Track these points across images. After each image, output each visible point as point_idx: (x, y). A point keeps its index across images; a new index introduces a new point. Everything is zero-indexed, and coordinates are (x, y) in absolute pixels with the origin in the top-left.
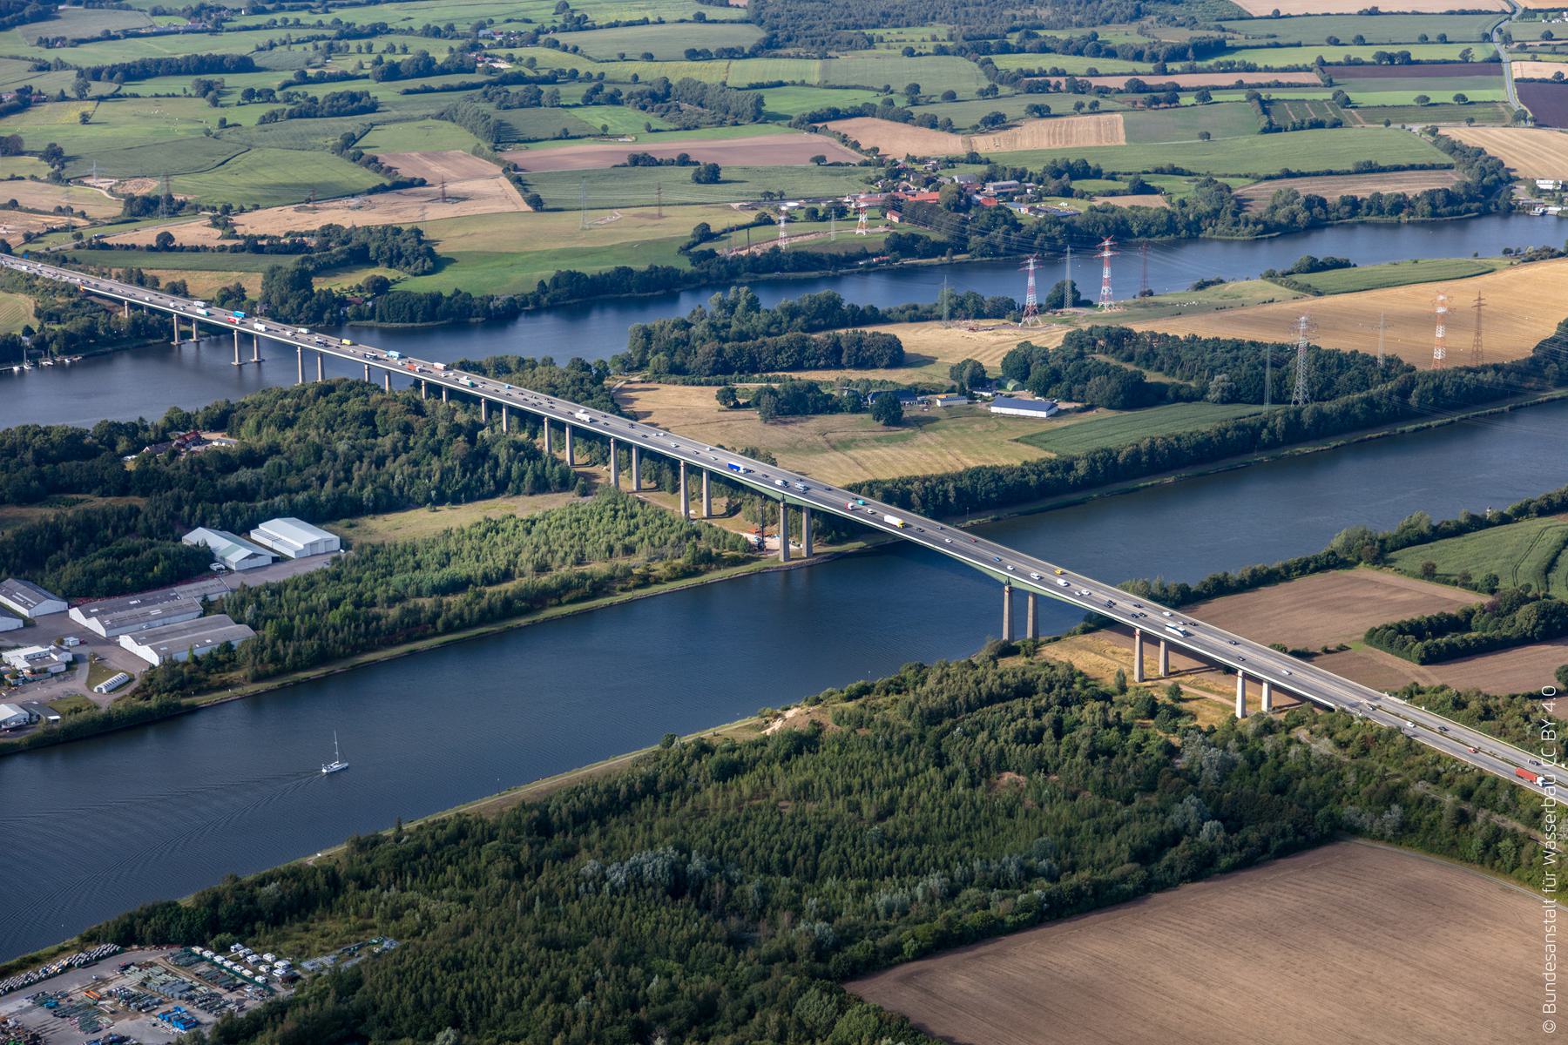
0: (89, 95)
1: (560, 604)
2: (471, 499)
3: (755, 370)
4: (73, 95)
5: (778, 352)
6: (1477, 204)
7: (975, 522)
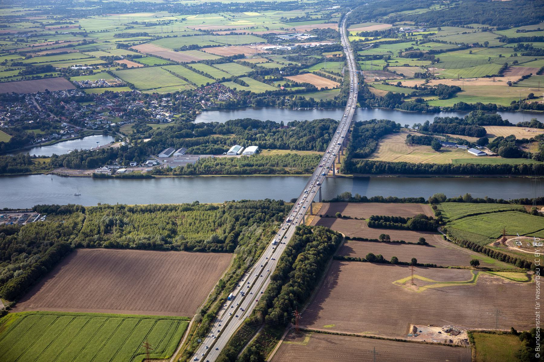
0: (489, 46)
1: (259, 174)
2: (303, 150)
3: (443, 133)
4: (484, 46)
5: (449, 128)
6: (340, 78)
7: (391, 176)
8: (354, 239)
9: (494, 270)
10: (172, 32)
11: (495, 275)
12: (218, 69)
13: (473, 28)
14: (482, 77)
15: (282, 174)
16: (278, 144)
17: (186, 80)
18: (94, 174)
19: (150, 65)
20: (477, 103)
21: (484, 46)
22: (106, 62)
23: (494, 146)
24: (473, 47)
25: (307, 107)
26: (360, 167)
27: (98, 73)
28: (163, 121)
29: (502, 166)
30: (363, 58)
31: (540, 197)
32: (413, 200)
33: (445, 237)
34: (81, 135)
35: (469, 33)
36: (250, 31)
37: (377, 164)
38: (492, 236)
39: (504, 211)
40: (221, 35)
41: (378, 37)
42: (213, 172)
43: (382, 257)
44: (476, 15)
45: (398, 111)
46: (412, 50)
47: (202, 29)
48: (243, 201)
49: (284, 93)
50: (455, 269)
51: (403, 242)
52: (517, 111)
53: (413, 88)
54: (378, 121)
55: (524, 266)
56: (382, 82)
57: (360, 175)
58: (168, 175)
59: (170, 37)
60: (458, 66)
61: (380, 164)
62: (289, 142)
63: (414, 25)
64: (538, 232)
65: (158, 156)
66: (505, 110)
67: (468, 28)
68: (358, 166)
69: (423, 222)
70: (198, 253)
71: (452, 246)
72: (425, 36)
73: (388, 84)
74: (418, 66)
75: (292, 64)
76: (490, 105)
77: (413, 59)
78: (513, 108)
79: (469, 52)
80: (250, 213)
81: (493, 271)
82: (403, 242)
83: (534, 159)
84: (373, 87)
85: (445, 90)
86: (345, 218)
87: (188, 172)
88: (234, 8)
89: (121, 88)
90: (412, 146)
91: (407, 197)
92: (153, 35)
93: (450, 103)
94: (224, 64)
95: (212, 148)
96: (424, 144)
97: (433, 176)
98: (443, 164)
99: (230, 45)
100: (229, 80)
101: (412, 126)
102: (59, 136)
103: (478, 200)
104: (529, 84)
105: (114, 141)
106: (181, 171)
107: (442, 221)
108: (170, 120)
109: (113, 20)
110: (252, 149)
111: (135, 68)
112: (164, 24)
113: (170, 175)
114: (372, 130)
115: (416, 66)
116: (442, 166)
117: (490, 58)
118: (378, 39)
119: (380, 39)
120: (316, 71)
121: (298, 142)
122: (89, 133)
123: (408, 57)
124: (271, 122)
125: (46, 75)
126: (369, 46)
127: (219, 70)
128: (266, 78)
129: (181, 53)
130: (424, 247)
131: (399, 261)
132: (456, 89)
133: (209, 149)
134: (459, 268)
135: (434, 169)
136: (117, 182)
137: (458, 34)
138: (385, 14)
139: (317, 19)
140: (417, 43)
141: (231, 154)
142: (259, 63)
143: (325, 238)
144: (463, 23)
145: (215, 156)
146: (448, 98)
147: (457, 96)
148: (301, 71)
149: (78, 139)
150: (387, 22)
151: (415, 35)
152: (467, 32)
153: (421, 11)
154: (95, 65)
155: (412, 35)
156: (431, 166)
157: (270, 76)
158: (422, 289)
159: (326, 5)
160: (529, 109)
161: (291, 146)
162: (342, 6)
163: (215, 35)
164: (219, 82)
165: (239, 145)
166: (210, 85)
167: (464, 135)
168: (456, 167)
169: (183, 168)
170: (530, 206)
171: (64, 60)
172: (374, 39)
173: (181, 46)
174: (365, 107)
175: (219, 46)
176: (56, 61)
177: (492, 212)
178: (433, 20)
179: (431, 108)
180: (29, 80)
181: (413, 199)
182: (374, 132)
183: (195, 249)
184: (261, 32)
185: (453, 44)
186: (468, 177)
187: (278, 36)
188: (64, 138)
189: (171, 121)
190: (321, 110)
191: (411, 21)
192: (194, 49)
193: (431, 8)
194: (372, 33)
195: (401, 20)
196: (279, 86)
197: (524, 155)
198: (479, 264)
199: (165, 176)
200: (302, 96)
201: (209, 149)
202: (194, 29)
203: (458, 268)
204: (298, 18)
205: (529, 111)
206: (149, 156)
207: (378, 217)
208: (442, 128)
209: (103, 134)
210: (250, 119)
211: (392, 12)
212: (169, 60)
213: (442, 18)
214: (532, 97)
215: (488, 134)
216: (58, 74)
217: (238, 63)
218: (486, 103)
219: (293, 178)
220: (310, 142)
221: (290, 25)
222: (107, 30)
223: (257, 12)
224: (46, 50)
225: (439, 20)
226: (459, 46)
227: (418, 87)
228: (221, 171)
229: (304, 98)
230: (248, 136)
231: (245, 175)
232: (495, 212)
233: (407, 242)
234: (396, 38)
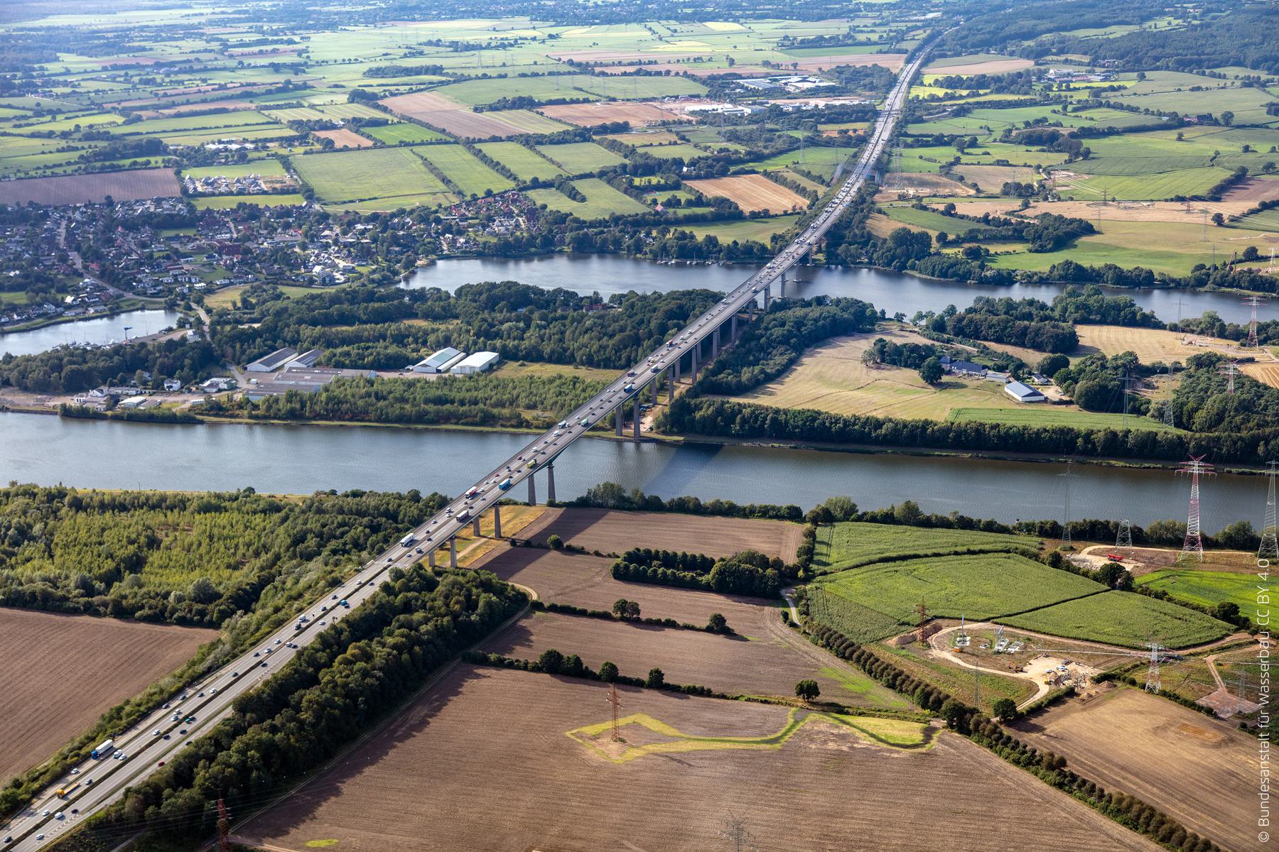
0: (1233, 123)
1: (457, 424)
2: (606, 367)
3: (978, 338)
4: (1222, 122)
5: (990, 328)
7: (776, 445)
8: (554, 608)
9: (851, 710)
10: (504, 65)
11: (848, 724)
12: (544, 156)
13: (1224, 77)
14: (1166, 200)
15: (512, 426)
16: (547, 349)
17: (446, 181)
18: (64, 406)
19: (388, 143)
20: (1106, 265)
21: (1222, 122)
22: (296, 134)
23: (1069, 379)
24: (1196, 124)
25: (691, 258)
26: (703, 417)
27: (259, 159)
28: (324, 280)
29: (1054, 431)
30: (909, 140)
31: (1088, 520)
32: (771, 513)
33: (786, 616)
34: (111, 309)
35: (1207, 89)
36: (681, 68)
37: (746, 411)
38: (906, 620)
39: (982, 552)
40: (612, 75)
41: (981, 92)
42: (346, 413)
43: (578, 660)
44: (1246, 45)
45: (912, 277)
46: (1043, 126)
47: (576, 59)
48: (356, 494)
49: (655, 221)
50: (755, 704)
51: (671, 624)
52: (1202, 289)
53: (978, 220)
54: (831, 301)
55: (930, 704)
56: (914, 202)
57: (701, 439)
58: (237, 416)
59: (490, 77)
60: (1127, 170)
61: (753, 412)
62: (576, 345)
63: (1089, 64)
64: (1028, 614)
65: (246, 369)
66: (1172, 285)
67: (1214, 76)
68: (698, 415)
69: (745, 570)
70: (142, 626)
71: (795, 638)
72: (1097, 92)
73: (925, 208)
74: (1030, 166)
75: (728, 150)
76: (1137, 272)
77: (1029, 148)
78: (1192, 282)
79: (1176, 136)
80: (341, 525)
81: (847, 713)
82: (671, 624)
83: (1153, 416)
84: (885, 214)
85: (1051, 230)
86: (572, 550)
87: (283, 412)
88: (689, 11)
89: (286, 196)
90: (878, 368)
91: (759, 502)
92: (450, 71)
93: (1043, 263)
94: (568, 145)
95: (378, 354)
96: (906, 366)
97: (881, 449)
98: (909, 418)
99: (614, 100)
100: (547, 185)
101: (912, 317)
102: (59, 310)
103: (934, 518)
104: (1270, 224)
105: (175, 327)
106: (269, 407)
107: (807, 570)
108: (342, 279)
109: (391, 35)
110: (480, 359)
111: (351, 150)
112: (503, 46)
113: (242, 417)
114: (795, 323)
115: (1025, 165)
116: (905, 426)
117: (1217, 153)
118: (980, 95)
119: (986, 94)
120: (769, 169)
121: (595, 348)
122: (133, 304)
123: (1020, 143)
124: (567, 292)
125: (135, 163)
126: (945, 111)
127: (544, 160)
128: (637, 181)
129: (487, 115)
130: (720, 639)
131: (621, 674)
132: (1079, 226)
133: (372, 354)
134: (766, 702)
135: (883, 432)
136: (119, 428)
137: (1180, 90)
138: (1030, 35)
139: (869, 43)
140: (1065, 108)
141: (424, 369)
142: (651, 145)
143: (458, 602)
144: (1206, 64)
145: (379, 373)
146: (1051, 250)
147: (1075, 246)
148: (733, 169)
149: (101, 317)
150: (1026, 54)
151: (1075, 89)
152: (1204, 87)
153: (1118, 32)
154: (260, 140)
155: (1068, 89)
156: (879, 424)
157: (647, 178)
158: (633, 754)
159: (914, 9)
160: (1233, 287)
161: (578, 356)
162: (945, 13)
163: (598, 75)
164: (521, 190)
165: (456, 348)
166: (494, 196)
167: (1023, 345)
168: (939, 430)
169: (277, 400)
170: (1057, 541)
171: (206, 128)
172: (968, 96)
173: (493, 98)
174: (837, 265)
175: (586, 101)
176: (185, 130)
177: (949, 554)
178: (1137, 53)
179: (988, 273)
180: (92, 173)
181: (773, 508)
182: (799, 329)
183: (138, 614)
184: (704, 71)
185: (1153, 113)
186: (967, 455)
187: (741, 81)
188: (69, 314)
189: (345, 282)
190: (729, 268)
191: (1085, 53)
192: (521, 107)
193: (1146, 25)
194: (972, 79)
195: (1061, 52)
196: (655, 202)
197: (1134, 407)
198: (818, 694)
199: (228, 420)
200: (687, 230)
201: (372, 354)
202: (560, 60)
203: (762, 702)
204: (821, 38)
205: (1229, 293)
206: (224, 367)
207: (648, 552)
208: (976, 326)
209: (164, 309)
210: (515, 284)
211: (1049, 31)
212: (444, 131)
213: (1160, 49)
214: (1252, 255)
215: (1084, 347)
216: (164, 161)
217: (600, 143)
218: (1127, 266)
219: (506, 439)
220: (625, 347)
221: (790, 54)
222: (356, 60)
223: (738, 22)
224: (188, 103)
225: (1149, 54)
226: (1165, 119)
227: (990, 218)
228: (367, 413)
229: (692, 237)
230: (481, 327)
231: (420, 426)
232: (956, 553)
233: (680, 622)
234: (1026, 94)
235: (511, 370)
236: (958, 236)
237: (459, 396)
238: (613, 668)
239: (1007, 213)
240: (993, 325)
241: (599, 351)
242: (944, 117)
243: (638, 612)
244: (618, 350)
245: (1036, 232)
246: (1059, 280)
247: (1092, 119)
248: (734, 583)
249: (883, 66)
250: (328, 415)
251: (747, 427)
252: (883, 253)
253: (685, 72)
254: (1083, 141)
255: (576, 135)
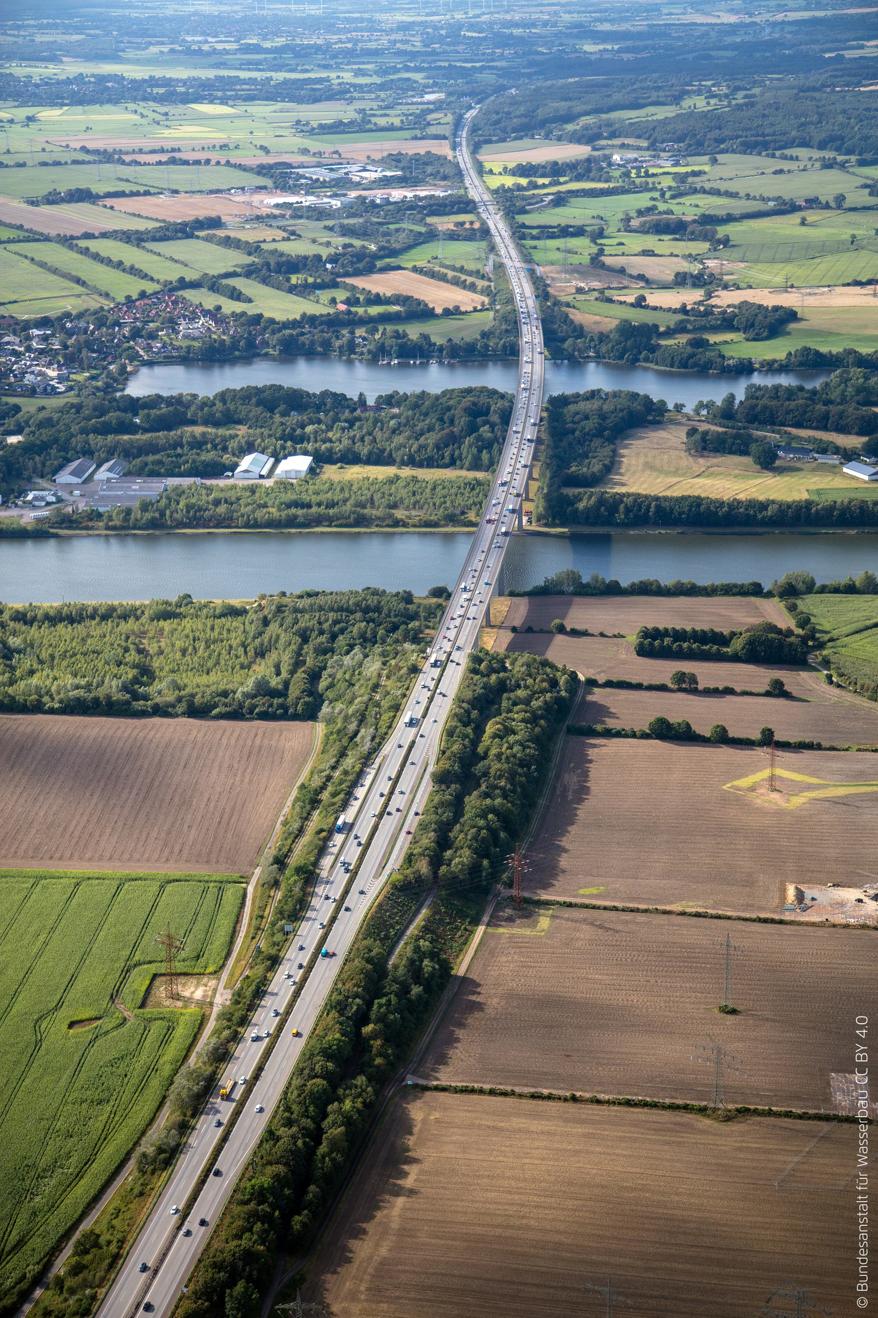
0: (845, 206)
1: (330, 526)
4: (833, 204)
5: (788, 413)
7: (663, 532)
14: (844, 285)
15: (388, 526)
20: (845, 350)
21: (833, 204)
25: (414, 357)
26: (586, 508)
28: (45, 389)
32: (734, 590)
35: (789, 171)
37: (628, 501)
40: (145, 164)
41: (562, 179)
42: (210, 520)
44: (803, 125)
45: (646, 369)
46: (653, 214)
49: (349, 320)
53: (675, 311)
57: (587, 530)
58: (92, 528)
60: (778, 256)
61: (635, 501)
68: (581, 505)
72: (682, 178)
73: (610, 301)
74: (677, 256)
82: (729, 691)
88: (161, 91)
94: (171, 242)
95: (194, 461)
96: (731, 452)
98: (790, 500)
99: (176, 192)
110: (299, 464)
115: (672, 255)
117: (854, 237)
118: (560, 184)
119: (565, 183)
121: (415, 447)
123: (647, 233)
126: (542, 201)
130: (781, 702)
131: (731, 735)
135: (769, 513)
137: (763, 173)
138: (570, 118)
139: (391, 128)
144: (772, 145)
147: (789, 333)
152: (786, 169)
161: (397, 456)
163: (129, 164)
165: (263, 452)
167: (825, 428)
168: (823, 509)
178: (695, 135)
181: (735, 586)
183: (215, 712)
185: (755, 198)
186: (853, 532)
190: (451, 366)
196: (333, 301)
199: (84, 532)
200: (400, 328)
202: (67, 146)
208: (771, 412)
211: (587, 113)
213: (717, 131)
220: (447, 446)
223: (227, 104)
225: (708, 136)
226: (771, 204)
228: (231, 519)
229: (405, 335)
235: (331, 472)
236: (668, 327)
237: (315, 499)
238: (724, 730)
239: (695, 303)
240: (791, 410)
241: (419, 450)
242: (545, 206)
243: (697, 683)
244: (437, 447)
245: (748, 321)
246: (799, 366)
247: (697, 206)
248: (765, 651)
249: (439, 153)
250: (190, 522)
251: (631, 515)
252: (613, 347)
253: (228, 162)
254: (718, 228)
255: (177, 231)
